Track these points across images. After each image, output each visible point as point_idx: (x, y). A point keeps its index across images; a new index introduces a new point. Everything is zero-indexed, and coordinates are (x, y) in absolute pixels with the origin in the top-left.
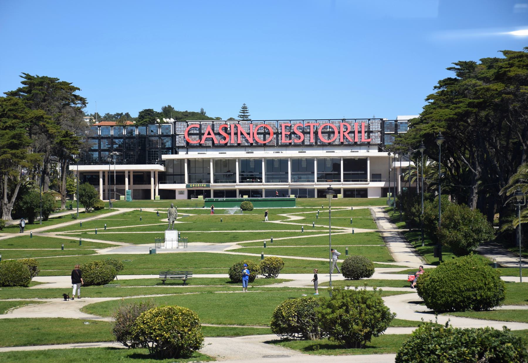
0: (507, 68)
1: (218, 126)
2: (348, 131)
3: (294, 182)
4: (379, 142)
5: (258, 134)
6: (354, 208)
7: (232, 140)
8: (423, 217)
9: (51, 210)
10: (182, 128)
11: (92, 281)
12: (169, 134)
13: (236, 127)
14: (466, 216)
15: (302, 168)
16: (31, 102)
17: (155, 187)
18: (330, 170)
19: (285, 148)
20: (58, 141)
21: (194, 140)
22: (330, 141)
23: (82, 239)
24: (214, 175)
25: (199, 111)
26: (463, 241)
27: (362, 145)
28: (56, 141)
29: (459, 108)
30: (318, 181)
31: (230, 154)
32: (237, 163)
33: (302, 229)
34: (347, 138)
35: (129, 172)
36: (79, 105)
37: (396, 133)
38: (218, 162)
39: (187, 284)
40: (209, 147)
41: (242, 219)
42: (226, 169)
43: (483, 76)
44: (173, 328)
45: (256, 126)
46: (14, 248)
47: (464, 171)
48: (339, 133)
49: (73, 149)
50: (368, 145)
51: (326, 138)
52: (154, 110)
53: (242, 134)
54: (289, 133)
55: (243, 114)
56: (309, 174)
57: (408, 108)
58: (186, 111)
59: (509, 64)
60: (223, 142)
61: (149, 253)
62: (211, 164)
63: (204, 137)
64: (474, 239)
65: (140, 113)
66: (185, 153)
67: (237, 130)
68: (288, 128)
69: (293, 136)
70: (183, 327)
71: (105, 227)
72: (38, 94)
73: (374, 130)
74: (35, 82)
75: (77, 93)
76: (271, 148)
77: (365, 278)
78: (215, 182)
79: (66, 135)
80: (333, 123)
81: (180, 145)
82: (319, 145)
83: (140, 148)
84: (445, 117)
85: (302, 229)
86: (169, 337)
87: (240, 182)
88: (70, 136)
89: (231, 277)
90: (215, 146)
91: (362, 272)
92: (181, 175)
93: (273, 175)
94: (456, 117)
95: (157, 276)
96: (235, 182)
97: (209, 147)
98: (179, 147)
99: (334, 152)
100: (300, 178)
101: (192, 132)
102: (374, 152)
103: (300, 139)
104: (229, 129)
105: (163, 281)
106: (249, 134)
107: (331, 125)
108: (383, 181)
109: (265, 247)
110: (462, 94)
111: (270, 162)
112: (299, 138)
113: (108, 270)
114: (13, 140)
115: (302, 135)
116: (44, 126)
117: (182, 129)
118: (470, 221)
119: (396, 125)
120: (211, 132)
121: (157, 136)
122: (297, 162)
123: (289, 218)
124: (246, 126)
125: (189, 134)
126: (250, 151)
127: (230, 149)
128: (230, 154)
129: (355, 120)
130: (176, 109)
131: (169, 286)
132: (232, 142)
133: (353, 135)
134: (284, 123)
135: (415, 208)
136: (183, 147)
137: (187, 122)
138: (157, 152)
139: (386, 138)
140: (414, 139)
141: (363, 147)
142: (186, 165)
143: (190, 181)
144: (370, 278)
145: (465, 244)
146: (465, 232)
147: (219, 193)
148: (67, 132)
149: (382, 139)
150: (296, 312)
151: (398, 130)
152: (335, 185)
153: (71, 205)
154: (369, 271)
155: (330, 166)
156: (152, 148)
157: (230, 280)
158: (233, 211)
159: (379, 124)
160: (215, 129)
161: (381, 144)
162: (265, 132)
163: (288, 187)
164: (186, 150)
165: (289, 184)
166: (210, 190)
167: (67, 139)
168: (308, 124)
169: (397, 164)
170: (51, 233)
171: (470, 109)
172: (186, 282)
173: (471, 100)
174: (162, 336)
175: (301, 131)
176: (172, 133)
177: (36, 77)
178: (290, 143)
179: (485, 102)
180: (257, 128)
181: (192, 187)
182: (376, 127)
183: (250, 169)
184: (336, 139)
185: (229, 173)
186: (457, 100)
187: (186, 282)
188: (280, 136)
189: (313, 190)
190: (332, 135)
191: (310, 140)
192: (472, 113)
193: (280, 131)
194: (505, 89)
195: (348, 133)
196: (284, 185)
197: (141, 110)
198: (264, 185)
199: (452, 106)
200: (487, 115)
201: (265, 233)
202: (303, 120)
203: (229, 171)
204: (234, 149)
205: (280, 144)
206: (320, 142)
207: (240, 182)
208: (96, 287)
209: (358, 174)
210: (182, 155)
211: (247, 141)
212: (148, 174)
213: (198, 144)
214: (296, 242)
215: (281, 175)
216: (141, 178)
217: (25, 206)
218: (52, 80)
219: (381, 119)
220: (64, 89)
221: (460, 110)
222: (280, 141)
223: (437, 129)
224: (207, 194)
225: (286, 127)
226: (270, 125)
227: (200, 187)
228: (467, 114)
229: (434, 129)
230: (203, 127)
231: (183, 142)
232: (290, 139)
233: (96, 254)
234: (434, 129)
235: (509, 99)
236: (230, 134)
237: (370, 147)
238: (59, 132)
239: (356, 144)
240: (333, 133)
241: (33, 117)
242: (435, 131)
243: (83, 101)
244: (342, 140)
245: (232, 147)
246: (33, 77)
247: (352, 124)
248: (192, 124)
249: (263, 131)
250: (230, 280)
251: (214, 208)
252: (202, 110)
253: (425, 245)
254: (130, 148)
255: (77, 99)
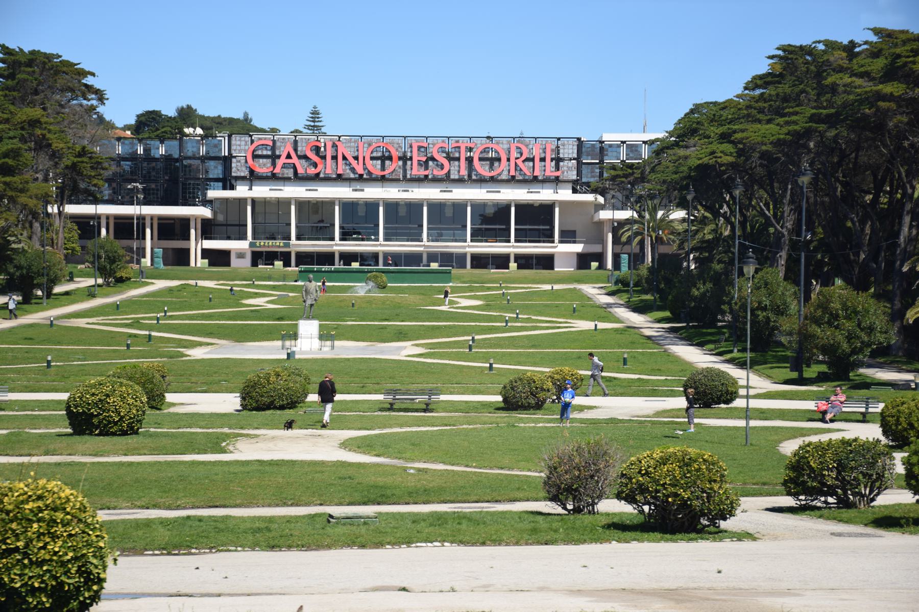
0: (908, 57)
1: (304, 144)
2: (523, 158)
3: (433, 241)
4: (575, 177)
5: (372, 158)
6: (556, 287)
7: (329, 168)
8: (736, 304)
9: (54, 281)
10: (241, 147)
11: (272, 402)
12: (219, 155)
13: (334, 146)
14: (849, 304)
15: (447, 217)
16: (15, 93)
17: (196, 245)
18: (492, 222)
19: (416, 184)
20: (69, 163)
21: (263, 167)
22: (493, 174)
23: (153, 334)
24: (297, 227)
25: (239, 115)
26: (845, 346)
27: (546, 181)
28: (67, 161)
29: (795, 123)
30: (472, 241)
31: (325, 192)
32: (337, 208)
33: (507, 322)
34: (521, 170)
35: (152, 218)
36: (94, 102)
37: (602, 162)
38: (302, 205)
39: (431, 411)
40: (289, 179)
41: (384, 303)
42: (317, 217)
43: (862, 69)
44: (695, 483)
45: (370, 145)
46: (38, 344)
47: (753, 227)
48: (508, 160)
49: (94, 177)
50: (556, 182)
51: (487, 168)
52: (163, 113)
53: (344, 158)
54: (424, 159)
55: (312, 124)
56: (414, 229)
57: (639, 123)
58: (219, 116)
59: (912, 51)
60: (312, 171)
61: (286, 357)
62: (293, 208)
63: (280, 163)
64: (862, 342)
65: (138, 116)
66: (247, 188)
67: (337, 151)
68: (422, 150)
69: (431, 163)
70: (710, 482)
71: (165, 312)
72: (28, 80)
73: (566, 156)
74: (23, 60)
75: (89, 80)
76: (394, 184)
77: (723, 406)
78: (299, 238)
79: (83, 153)
80: (498, 143)
81: (239, 174)
82: (475, 181)
83: (167, 178)
84: (771, 139)
85: (507, 322)
86: (688, 498)
87: (341, 239)
88: (91, 156)
89: (505, 400)
90: (298, 178)
91: (721, 395)
92: (239, 225)
93: (396, 228)
94: (789, 137)
95: (381, 397)
96: (333, 239)
97: (289, 179)
98: (237, 178)
99: (499, 192)
100: (441, 235)
101: (259, 152)
102: (565, 194)
103: (442, 169)
104: (322, 149)
105: (392, 404)
106: (356, 158)
107: (495, 147)
108: (580, 242)
109: (470, 350)
110: (795, 100)
111: (392, 207)
112: (442, 167)
113: (298, 385)
114: (7, 160)
115: (445, 162)
116: (44, 136)
117: (243, 147)
118: (856, 313)
119: (602, 149)
120: (293, 154)
121: (199, 158)
122: (437, 208)
123: (458, 303)
124: (353, 144)
125: (255, 157)
126: (358, 187)
127: (323, 183)
128: (325, 192)
129: (536, 138)
130: (201, 112)
131: (402, 413)
132: (329, 171)
133: (531, 164)
134: (417, 141)
135: (698, 289)
136: (243, 178)
137: (251, 136)
138: (198, 185)
139: (585, 170)
140: (676, 173)
141: (547, 184)
142: (249, 209)
143: (255, 237)
144: (730, 406)
145: (848, 350)
146: (848, 330)
147: (304, 258)
148: (84, 148)
149: (579, 173)
150: (834, 462)
151: (605, 158)
152: (453, 247)
153: (71, 273)
154: (731, 393)
155: (404, 214)
156: (190, 179)
157: (502, 405)
158: (361, 289)
159: (575, 147)
160: (299, 149)
161: (578, 180)
162: (383, 156)
163: (422, 249)
164: (248, 182)
165: (424, 245)
166: (290, 253)
167: (85, 159)
168: (457, 145)
169: (605, 215)
170: (72, 320)
171: (814, 125)
172: (430, 407)
173: (814, 111)
174: (676, 495)
175: (444, 155)
176: (225, 152)
177: (17, 50)
178: (426, 176)
179: (837, 114)
180: (371, 149)
181: (260, 246)
182: (571, 151)
183: (359, 220)
184: (503, 170)
185: (322, 225)
186: (791, 110)
187: (430, 407)
188: (409, 163)
189: (464, 256)
190: (496, 164)
191: (459, 172)
192: (816, 131)
193: (409, 154)
194: (907, 93)
195: (524, 161)
196: (416, 246)
197: (140, 112)
198: (380, 245)
199: (781, 120)
200: (837, 135)
201: (445, 326)
202: (449, 138)
203: (322, 221)
204: (330, 183)
205: (408, 176)
206: (476, 175)
207: (341, 239)
208: (278, 412)
209: (495, 229)
210: (241, 191)
211: (353, 170)
212: (184, 223)
213: (269, 174)
214: (498, 343)
215: (410, 229)
216: (173, 230)
217: (18, 274)
218: (49, 57)
219: (579, 139)
220: (67, 74)
221: (797, 128)
222: (409, 172)
223: (720, 157)
224: (286, 258)
225: (419, 148)
226: (392, 143)
227: (272, 246)
228: (808, 133)
229: (716, 157)
230: (278, 144)
231: (244, 169)
232: (427, 168)
233: (184, 358)
234: (716, 157)
235: (888, 110)
236: (324, 158)
237: (560, 184)
238: (69, 148)
239: (535, 179)
240: (499, 160)
241: (25, 121)
242: (719, 160)
243: (101, 96)
244: (512, 173)
245: (327, 179)
246: (14, 50)
247: (531, 147)
248: (260, 139)
249: (379, 154)
250: (502, 405)
251: (327, 284)
252: (246, 114)
253: (739, 351)
254: (150, 177)
255: (89, 91)
